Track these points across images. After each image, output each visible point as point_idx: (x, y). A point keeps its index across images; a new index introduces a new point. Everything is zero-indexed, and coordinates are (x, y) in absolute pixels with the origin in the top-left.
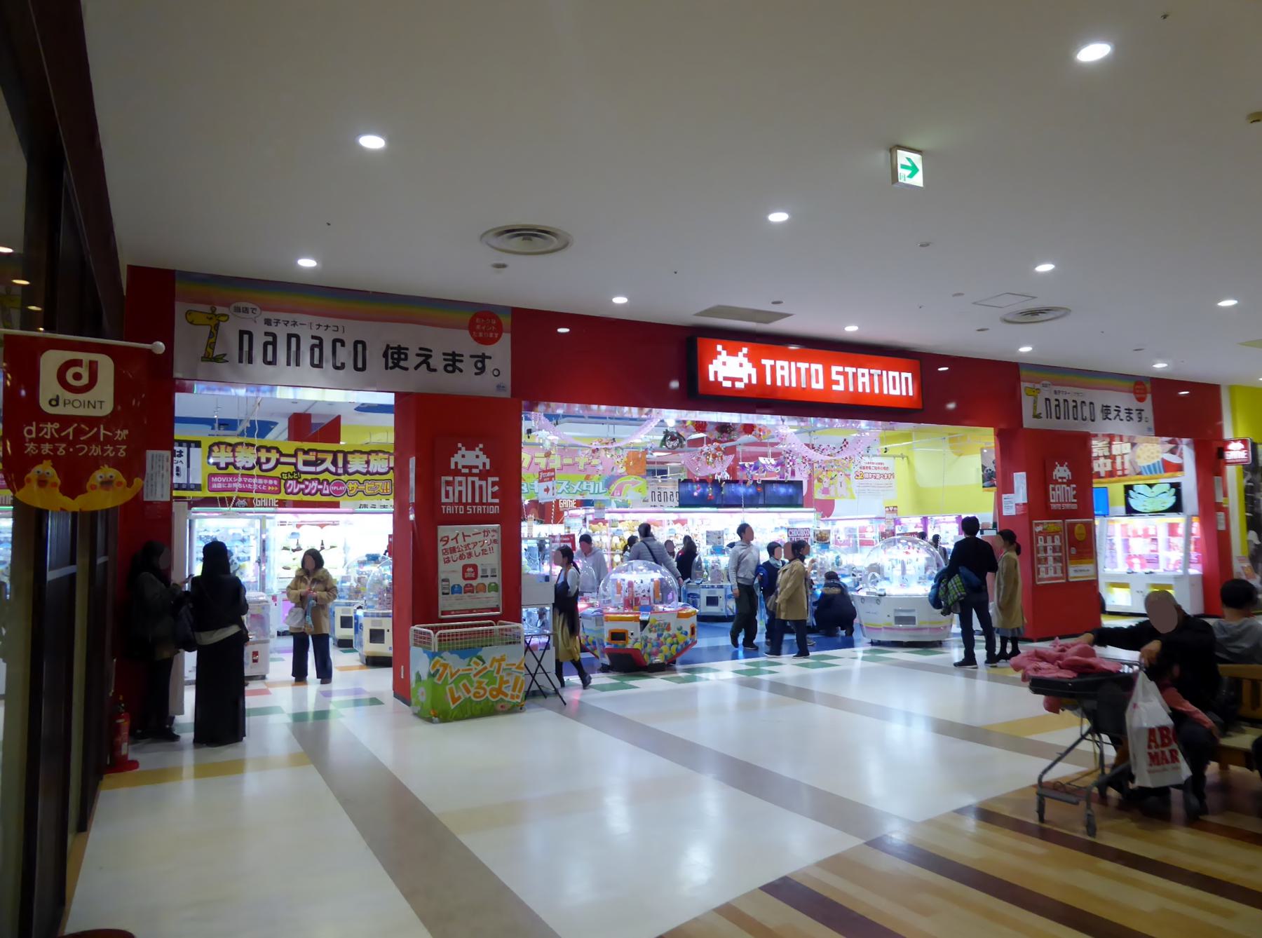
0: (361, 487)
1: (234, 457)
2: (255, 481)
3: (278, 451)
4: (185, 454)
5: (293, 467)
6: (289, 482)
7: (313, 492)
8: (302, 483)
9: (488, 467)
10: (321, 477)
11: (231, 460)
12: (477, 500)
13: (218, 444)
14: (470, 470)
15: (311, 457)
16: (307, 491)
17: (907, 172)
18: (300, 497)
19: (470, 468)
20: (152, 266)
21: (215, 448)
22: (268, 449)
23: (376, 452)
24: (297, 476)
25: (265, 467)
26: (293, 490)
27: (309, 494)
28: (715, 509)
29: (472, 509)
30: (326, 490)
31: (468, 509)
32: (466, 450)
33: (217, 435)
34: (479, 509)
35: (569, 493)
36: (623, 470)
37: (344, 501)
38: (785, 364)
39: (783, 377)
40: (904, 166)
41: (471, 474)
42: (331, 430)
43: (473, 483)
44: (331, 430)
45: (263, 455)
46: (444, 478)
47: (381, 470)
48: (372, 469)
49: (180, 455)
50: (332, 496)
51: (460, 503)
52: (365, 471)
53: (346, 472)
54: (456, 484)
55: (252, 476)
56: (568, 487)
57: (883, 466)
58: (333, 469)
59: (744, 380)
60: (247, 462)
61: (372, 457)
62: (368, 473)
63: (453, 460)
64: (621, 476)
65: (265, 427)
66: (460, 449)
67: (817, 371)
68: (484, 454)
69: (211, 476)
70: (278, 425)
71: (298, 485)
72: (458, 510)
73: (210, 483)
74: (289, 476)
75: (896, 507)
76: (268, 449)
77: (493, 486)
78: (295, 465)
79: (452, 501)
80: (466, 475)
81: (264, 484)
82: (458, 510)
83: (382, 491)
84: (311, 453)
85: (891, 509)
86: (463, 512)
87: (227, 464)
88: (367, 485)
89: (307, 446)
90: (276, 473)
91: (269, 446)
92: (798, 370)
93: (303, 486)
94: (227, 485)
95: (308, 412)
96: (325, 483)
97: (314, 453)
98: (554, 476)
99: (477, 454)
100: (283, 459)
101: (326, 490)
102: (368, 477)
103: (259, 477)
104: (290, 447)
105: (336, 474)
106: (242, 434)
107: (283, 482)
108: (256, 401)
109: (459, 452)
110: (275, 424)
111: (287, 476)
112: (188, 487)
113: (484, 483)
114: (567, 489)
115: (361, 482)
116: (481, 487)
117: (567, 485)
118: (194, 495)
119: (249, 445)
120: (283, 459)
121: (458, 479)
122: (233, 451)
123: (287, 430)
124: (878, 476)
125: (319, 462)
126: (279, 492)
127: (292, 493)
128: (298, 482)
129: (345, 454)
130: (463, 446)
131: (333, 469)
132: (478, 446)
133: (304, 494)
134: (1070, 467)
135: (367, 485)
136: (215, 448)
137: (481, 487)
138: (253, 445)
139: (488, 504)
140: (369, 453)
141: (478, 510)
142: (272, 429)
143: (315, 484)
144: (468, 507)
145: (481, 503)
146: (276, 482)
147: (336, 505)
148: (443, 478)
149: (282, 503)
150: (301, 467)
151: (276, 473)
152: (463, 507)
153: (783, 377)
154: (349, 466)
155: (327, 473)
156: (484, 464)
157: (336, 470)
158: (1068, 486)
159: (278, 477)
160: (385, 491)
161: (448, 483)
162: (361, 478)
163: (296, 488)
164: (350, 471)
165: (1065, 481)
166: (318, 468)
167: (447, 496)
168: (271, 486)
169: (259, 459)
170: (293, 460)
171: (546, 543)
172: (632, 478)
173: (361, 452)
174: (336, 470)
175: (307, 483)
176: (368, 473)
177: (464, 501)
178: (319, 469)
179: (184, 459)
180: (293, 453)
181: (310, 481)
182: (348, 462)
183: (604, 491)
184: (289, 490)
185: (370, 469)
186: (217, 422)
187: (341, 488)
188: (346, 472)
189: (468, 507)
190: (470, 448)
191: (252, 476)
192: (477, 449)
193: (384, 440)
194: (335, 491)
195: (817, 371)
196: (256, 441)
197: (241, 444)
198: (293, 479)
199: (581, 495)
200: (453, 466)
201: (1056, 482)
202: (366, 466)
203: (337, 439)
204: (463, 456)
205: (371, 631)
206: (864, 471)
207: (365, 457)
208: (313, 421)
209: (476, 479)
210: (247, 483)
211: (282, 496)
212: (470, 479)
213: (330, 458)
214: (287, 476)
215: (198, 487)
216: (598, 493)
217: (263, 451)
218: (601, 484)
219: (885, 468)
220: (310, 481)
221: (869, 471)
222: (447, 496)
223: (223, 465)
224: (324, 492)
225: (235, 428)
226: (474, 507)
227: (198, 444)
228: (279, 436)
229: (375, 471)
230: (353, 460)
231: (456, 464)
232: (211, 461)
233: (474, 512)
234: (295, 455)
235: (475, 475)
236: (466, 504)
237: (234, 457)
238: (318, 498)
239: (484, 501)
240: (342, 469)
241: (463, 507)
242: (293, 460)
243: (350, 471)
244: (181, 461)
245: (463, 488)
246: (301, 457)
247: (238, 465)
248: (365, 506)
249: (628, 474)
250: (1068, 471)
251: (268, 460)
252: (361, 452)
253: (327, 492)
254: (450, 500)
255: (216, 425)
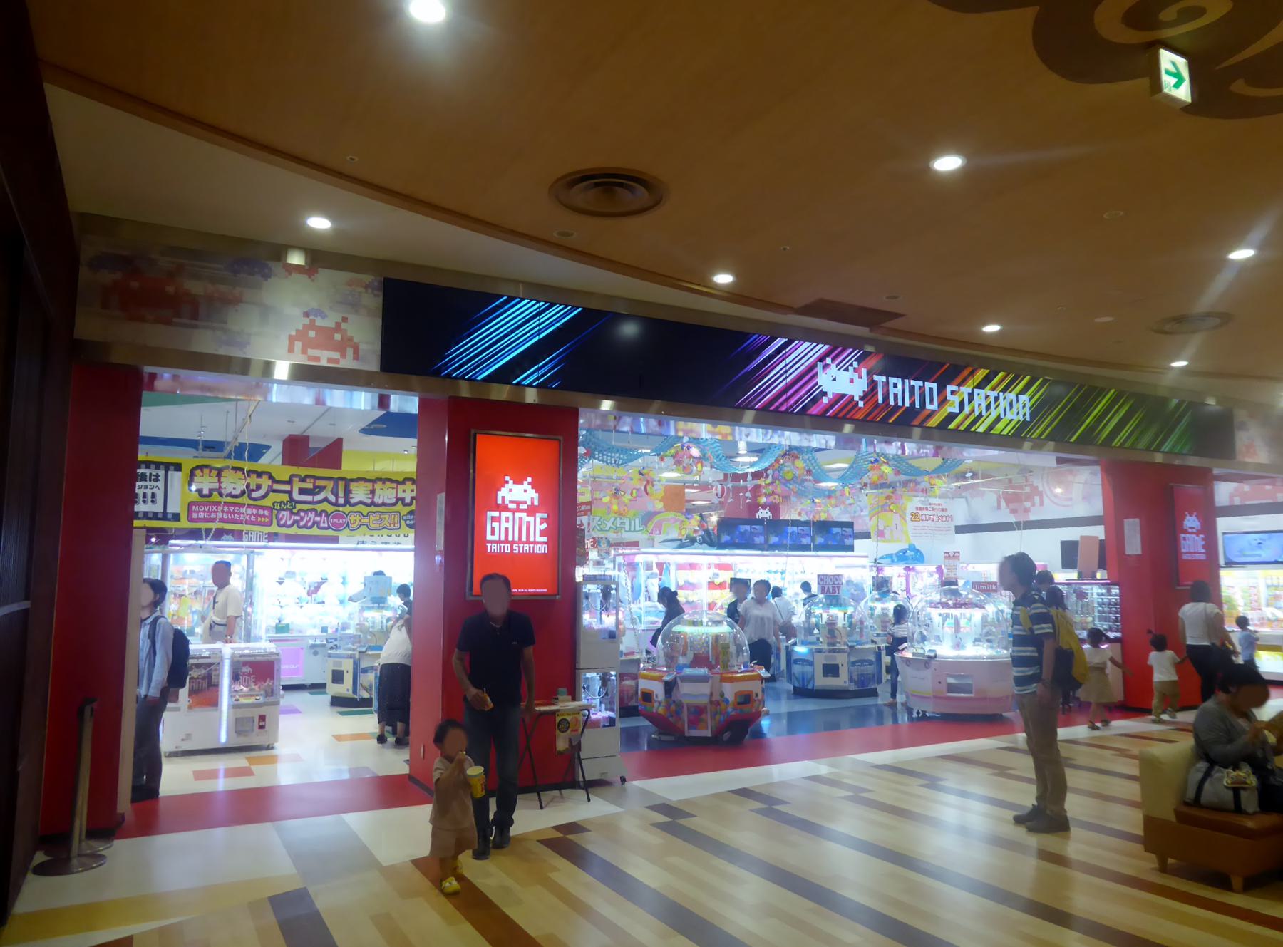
0: (366, 520)
1: (220, 482)
2: (243, 510)
3: (271, 477)
4: (162, 478)
5: (287, 495)
6: (283, 513)
7: (309, 524)
8: (297, 514)
9: (536, 503)
10: (319, 507)
11: (216, 486)
12: (524, 539)
13: (201, 467)
14: (518, 506)
15: (308, 485)
16: (302, 524)
17: (1173, 80)
18: (294, 530)
19: (518, 503)
20: (691, 322)
21: (198, 472)
22: (259, 475)
23: (384, 481)
24: (292, 505)
25: (255, 495)
26: (286, 521)
27: (305, 527)
28: (759, 552)
29: (519, 547)
30: (324, 522)
31: (514, 548)
32: (514, 483)
33: (202, 457)
34: (526, 547)
35: (602, 530)
36: (660, 506)
37: (343, 535)
38: (899, 381)
39: (896, 396)
40: (1167, 72)
41: (519, 510)
42: (332, 454)
43: (521, 519)
44: (332, 454)
45: (253, 481)
46: (490, 514)
47: (387, 501)
48: (378, 500)
49: (157, 480)
50: (330, 530)
51: (506, 541)
52: (369, 501)
53: (347, 502)
54: (503, 520)
55: (242, 505)
56: (600, 523)
57: (940, 507)
58: (332, 498)
59: (828, 394)
60: (234, 489)
61: (378, 486)
62: (373, 504)
63: (500, 494)
64: (656, 513)
65: (257, 451)
66: (507, 482)
67: (931, 389)
68: (532, 488)
69: (191, 504)
70: (271, 449)
71: (293, 517)
72: (504, 549)
73: (190, 512)
74: (282, 505)
75: (959, 552)
76: (259, 475)
77: (541, 524)
78: (290, 493)
79: (497, 539)
80: (513, 511)
81: (253, 514)
82: (504, 549)
83: (388, 525)
84: (308, 480)
85: (952, 554)
86: (509, 551)
87: (211, 491)
88: (372, 518)
89: (303, 471)
90: (267, 502)
91: (259, 470)
92: (912, 388)
93: (297, 518)
94: (210, 515)
95: (305, 434)
96: (324, 515)
97: (312, 480)
98: (590, 510)
99: (525, 488)
100: (276, 486)
101: (324, 522)
102: (373, 509)
103: (249, 506)
104: (284, 472)
105: (336, 504)
106: (228, 457)
107: (275, 512)
108: (247, 414)
109: (506, 485)
110: (268, 448)
111: (280, 506)
112: (164, 516)
113: (531, 519)
114: (599, 525)
115: (365, 514)
116: (528, 523)
117: (599, 521)
118: (177, 527)
119: (236, 469)
120: (276, 486)
121: (504, 514)
122: (219, 475)
123: (281, 456)
124: (936, 518)
125: (317, 490)
126: (270, 524)
127: (285, 525)
128: (292, 513)
129: (348, 482)
130: (511, 479)
131: (332, 498)
132: (526, 480)
133: (299, 527)
134: (1198, 517)
135: (372, 518)
136: (198, 472)
137: (528, 523)
138: (242, 470)
139: (535, 542)
140: (373, 481)
141: (525, 548)
142: (264, 453)
143: (312, 515)
144: (515, 545)
145: (528, 542)
146: (266, 513)
147: (335, 540)
148: (488, 513)
149: (272, 537)
150: (296, 496)
151: (267, 502)
152: (509, 545)
153: (896, 396)
154: (351, 496)
155: (325, 503)
156: (532, 499)
157: (337, 500)
158: (1197, 535)
159: (270, 507)
160: (392, 525)
161: (493, 519)
162: (365, 510)
163: (290, 520)
164: (353, 501)
165: (1194, 530)
166: (315, 497)
167: (493, 533)
168: (261, 516)
169: (248, 486)
170: (287, 487)
171: (613, 589)
172: (671, 515)
173: (391, 481)
174: (337, 500)
175: (302, 514)
176: (373, 504)
177: (510, 539)
178: (318, 498)
179: (161, 484)
180: (287, 478)
181: (306, 512)
182: (350, 492)
183: (642, 528)
184: (282, 522)
185: (376, 500)
186: (201, 444)
187: (341, 521)
188: (347, 502)
189: (515, 545)
190: (518, 481)
191: (242, 505)
192: (526, 483)
193: (408, 470)
194: (334, 524)
195: (931, 389)
196: (247, 466)
197: (227, 468)
198: (287, 509)
199: (614, 532)
200: (499, 501)
201: (1186, 532)
202: (371, 496)
203: (337, 464)
204: (511, 490)
205: (825, 666)
206: (921, 512)
207: (370, 485)
208: (311, 445)
209: (524, 515)
210: (234, 513)
211: (274, 528)
212: (518, 515)
213: (330, 485)
214: (280, 506)
215: (176, 517)
216: (635, 531)
217: (254, 476)
218: (637, 520)
219: (943, 510)
220: (306, 512)
221: (926, 512)
222: (493, 533)
223: (206, 492)
224: (322, 525)
225: (221, 451)
226: (521, 545)
227: (178, 467)
228: (272, 460)
229: (380, 502)
230: (356, 489)
231: (503, 498)
232: (194, 488)
233: (521, 551)
234: (289, 482)
235: (522, 511)
236: (512, 543)
237: (220, 482)
238: (315, 531)
239: (532, 539)
240: (343, 499)
241: (509, 545)
242: (287, 487)
243: (353, 501)
244: (157, 486)
245: (510, 525)
246: (297, 485)
247: (225, 492)
248: (363, 543)
249: (666, 511)
250: (1197, 521)
251: (259, 487)
252: (391, 481)
253: (326, 525)
254: (496, 538)
255: (200, 447)
